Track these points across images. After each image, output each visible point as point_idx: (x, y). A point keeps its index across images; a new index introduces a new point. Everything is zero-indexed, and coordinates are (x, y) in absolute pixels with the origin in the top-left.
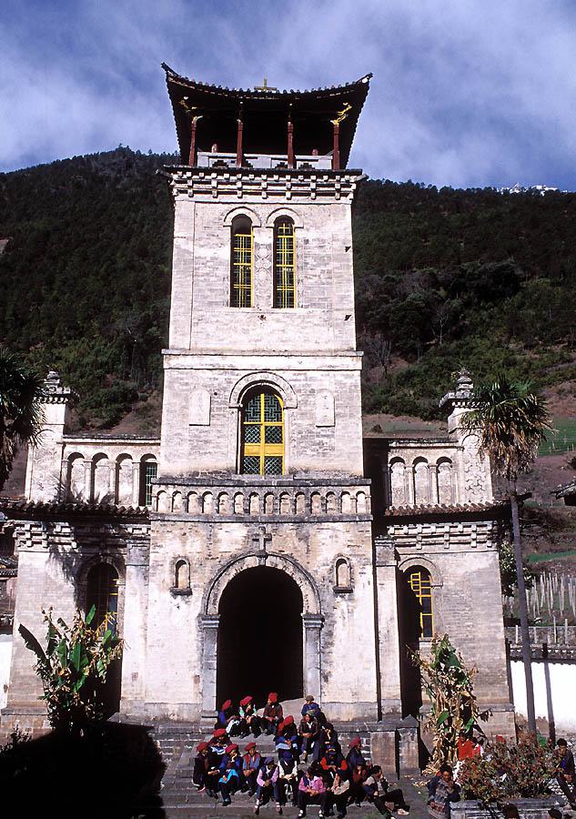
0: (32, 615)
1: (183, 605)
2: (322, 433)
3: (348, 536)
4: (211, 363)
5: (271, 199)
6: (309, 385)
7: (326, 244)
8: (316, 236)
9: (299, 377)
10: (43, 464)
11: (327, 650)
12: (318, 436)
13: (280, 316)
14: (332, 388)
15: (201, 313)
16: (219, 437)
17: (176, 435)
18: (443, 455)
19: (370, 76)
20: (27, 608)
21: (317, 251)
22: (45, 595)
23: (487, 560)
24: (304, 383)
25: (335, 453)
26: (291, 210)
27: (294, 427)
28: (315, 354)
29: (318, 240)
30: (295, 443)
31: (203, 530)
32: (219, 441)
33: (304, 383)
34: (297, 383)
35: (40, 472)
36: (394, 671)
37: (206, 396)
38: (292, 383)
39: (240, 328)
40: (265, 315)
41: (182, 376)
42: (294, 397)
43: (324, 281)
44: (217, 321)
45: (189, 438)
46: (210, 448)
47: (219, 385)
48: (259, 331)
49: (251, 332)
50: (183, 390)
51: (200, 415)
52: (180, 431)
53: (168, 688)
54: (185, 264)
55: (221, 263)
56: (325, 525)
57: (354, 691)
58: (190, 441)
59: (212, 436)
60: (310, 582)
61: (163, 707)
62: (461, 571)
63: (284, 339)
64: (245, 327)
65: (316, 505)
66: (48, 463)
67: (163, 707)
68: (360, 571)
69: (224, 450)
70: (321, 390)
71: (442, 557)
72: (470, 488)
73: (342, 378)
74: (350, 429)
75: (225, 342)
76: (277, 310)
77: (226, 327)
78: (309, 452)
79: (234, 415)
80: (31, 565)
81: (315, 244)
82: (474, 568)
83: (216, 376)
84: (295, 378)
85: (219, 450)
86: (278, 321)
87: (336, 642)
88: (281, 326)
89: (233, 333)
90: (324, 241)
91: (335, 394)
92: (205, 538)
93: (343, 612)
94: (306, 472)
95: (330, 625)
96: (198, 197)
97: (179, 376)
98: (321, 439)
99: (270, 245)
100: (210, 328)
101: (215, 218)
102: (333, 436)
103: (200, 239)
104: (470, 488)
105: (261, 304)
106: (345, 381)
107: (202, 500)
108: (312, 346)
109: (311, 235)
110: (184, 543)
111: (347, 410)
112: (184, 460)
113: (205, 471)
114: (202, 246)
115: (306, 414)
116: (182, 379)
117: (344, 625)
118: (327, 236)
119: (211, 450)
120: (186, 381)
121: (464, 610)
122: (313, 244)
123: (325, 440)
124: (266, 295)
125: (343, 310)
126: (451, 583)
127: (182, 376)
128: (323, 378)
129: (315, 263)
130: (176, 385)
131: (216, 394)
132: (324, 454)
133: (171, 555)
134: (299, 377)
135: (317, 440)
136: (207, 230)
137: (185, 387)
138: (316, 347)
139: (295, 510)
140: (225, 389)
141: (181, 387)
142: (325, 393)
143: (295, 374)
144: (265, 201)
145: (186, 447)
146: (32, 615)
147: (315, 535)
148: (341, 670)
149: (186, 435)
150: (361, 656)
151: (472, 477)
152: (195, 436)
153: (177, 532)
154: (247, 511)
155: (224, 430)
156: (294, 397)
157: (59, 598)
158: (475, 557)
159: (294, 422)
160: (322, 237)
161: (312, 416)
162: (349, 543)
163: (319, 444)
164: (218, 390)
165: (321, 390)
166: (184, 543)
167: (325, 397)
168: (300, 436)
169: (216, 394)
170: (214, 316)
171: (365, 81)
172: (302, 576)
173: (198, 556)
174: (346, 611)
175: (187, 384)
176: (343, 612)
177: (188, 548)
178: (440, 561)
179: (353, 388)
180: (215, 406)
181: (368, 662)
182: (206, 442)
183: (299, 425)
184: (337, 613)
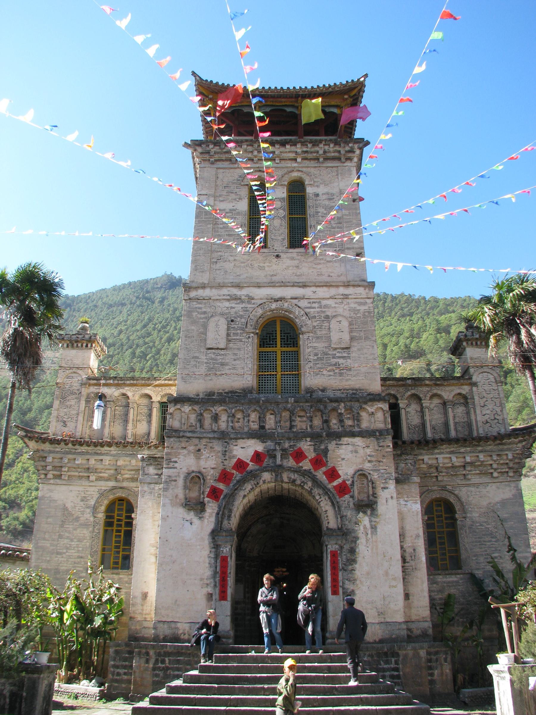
0: (48, 545)
1: (196, 521)
2: (338, 355)
3: (368, 451)
4: (227, 293)
5: (284, 164)
6: (324, 312)
7: (335, 197)
8: (326, 190)
9: (314, 305)
10: (68, 403)
11: (350, 567)
12: (333, 358)
13: (295, 255)
14: (347, 314)
15: (219, 253)
16: (235, 360)
17: (193, 358)
18: (459, 392)
19: (366, 76)
20: (44, 539)
21: (327, 202)
22: (62, 526)
23: (511, 491)
24: (319, 310)
25: (351, 373)
26: (302, 171)
27: (309, 350)
28: (328, 285)
29: (328, 194)
30: (312, 364)
31: (218, 446)
32: (234, 363)
33: (319, 310)
34: (312, 310)
35: (65, 410)
36: (422, 591)
37: (223, 324)
38: (307, 310)
39: (256, 265)
40: (280, 254)
41: (200, 306)
42: (309, 322)
43: (334, 226)
44: (235, 260)
45: (206, 361)
46: (226, 370)
47: (236, 313)
48: (274, 267)
49: (267, 269)
50: (201, 318)
51: (217, 339)
52: (196, 355)
53: (178, 605)
54: (206, 215)
55: (239, 214)
56: (345, 440)
57: (381, 610)
58: (206, 363)
59: (229, 358)
60: (330, 498)
61: (173, 625)
62: (484, 503)
63: (298, 274)
64: (262, 265)
65: (334, 422)
66: (73, 402)
67: (173, 625)
68: (382, 486)
69: (241, 371)
70: (335, 316)
71: (464, 489)
72: (487, 422)
73: (356, 305)
74: (365, 351)
75: (242, 277)
76: (291, 250)
77: (243, 265)
78: (325, 372)
79: (250, 340)
80: (50, 497)
81: (325, 197)
82: (497, 499)
83: (233, 305)
84: (309, 305)
85: (235, 371)
86: (292, 259)
87: (359, 559)
88: (296, 262)
89: (250, 270)
90: (333, 195)
91: (350, 320)
92: (220, 454)
93: (365, 527)
94: (323, 390)
95: (352, 541)
96: (220, 164)
97: (198, 306)
98: (338, 360)
99: (283, 199)
100: (229, 266)
101: (234, 180)
102: (349, 357)
103: (220, 196)
104: (487, 422)
105: (275, 246)
106: (358, 308)
107: (216, 418)
108: (325, 278)
109: (321, 190)
110: (198, 458)
111: (362, 334)
112: (200, 381)
113: (221, 391)
114: (222, 201)
115: (321, 337)
116: (200, 308)
117: (367, 540)
118: (335, 191)
119: (228, 372)
120: (204, 310)
121: (490, 541)
122: (321, 197)
123: (341, 361)
124: (280, 238)
125: (353, 248)
126: (476, 515)
127: (200, 306)
128: (337, 305)
129: (325, 212)
130: (194, 314)
131: (232, 321)
132: (341, 374)
133: (185, 470)
134: (314, 305)
135: (333, 361)
136: (227, 189)
137: (203, 316)
138: (329, 279)
139: (311, 426)
140: (241, 317)
141: (199, 316)
142: (340, 319)
143: (310, 303)
144: (279, 165)
145: (203, 369)
146: (48, 545)
147: (334, 451)
148: (364, 588)
149: (203, 358)
150: (387, 574)
151: (488, 412)
152: (212, 359)
153: (192, 448)
154: (262, 427)
155: (241, 354)
156: (309, 322)
157: (75, 529)
158: (498, 488)
159: (309, 345)
160: (331, 191)
161: (329, 339)
162: (369, 458)
163: (335, 365)
164: (235, 317)
165: (335, 316)
166: (198, 458)
167: (340, 322)
168: (316, 358)
169: (232, 321)
170: (231, 256)
171: (362, 79)
172: (321, 492)
173: (212, 472)
174: (368, 525)
175: (205, 313)
176: (365, 527)
177: (202, 463)
178: (463, 492)
179: (367, 314)
180: (232, 331)
181: (394, 579)
182: (222, 364)
183: (315, 348)
184: (360, 531)
